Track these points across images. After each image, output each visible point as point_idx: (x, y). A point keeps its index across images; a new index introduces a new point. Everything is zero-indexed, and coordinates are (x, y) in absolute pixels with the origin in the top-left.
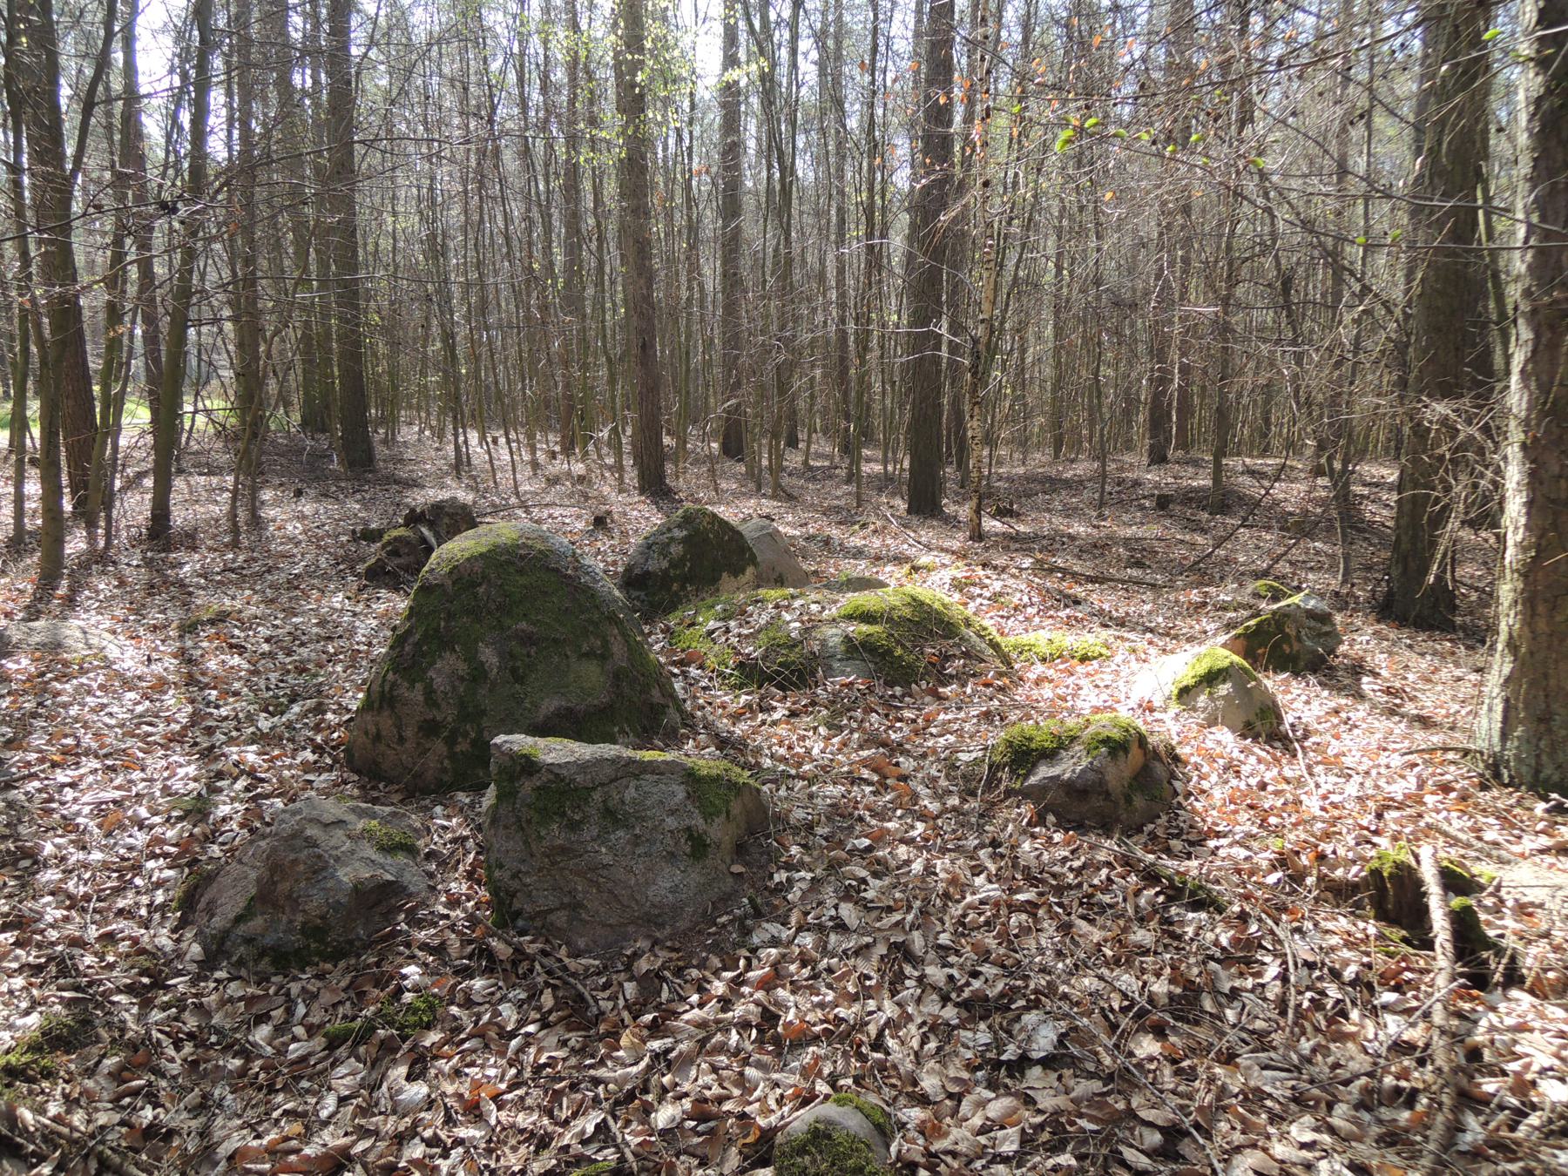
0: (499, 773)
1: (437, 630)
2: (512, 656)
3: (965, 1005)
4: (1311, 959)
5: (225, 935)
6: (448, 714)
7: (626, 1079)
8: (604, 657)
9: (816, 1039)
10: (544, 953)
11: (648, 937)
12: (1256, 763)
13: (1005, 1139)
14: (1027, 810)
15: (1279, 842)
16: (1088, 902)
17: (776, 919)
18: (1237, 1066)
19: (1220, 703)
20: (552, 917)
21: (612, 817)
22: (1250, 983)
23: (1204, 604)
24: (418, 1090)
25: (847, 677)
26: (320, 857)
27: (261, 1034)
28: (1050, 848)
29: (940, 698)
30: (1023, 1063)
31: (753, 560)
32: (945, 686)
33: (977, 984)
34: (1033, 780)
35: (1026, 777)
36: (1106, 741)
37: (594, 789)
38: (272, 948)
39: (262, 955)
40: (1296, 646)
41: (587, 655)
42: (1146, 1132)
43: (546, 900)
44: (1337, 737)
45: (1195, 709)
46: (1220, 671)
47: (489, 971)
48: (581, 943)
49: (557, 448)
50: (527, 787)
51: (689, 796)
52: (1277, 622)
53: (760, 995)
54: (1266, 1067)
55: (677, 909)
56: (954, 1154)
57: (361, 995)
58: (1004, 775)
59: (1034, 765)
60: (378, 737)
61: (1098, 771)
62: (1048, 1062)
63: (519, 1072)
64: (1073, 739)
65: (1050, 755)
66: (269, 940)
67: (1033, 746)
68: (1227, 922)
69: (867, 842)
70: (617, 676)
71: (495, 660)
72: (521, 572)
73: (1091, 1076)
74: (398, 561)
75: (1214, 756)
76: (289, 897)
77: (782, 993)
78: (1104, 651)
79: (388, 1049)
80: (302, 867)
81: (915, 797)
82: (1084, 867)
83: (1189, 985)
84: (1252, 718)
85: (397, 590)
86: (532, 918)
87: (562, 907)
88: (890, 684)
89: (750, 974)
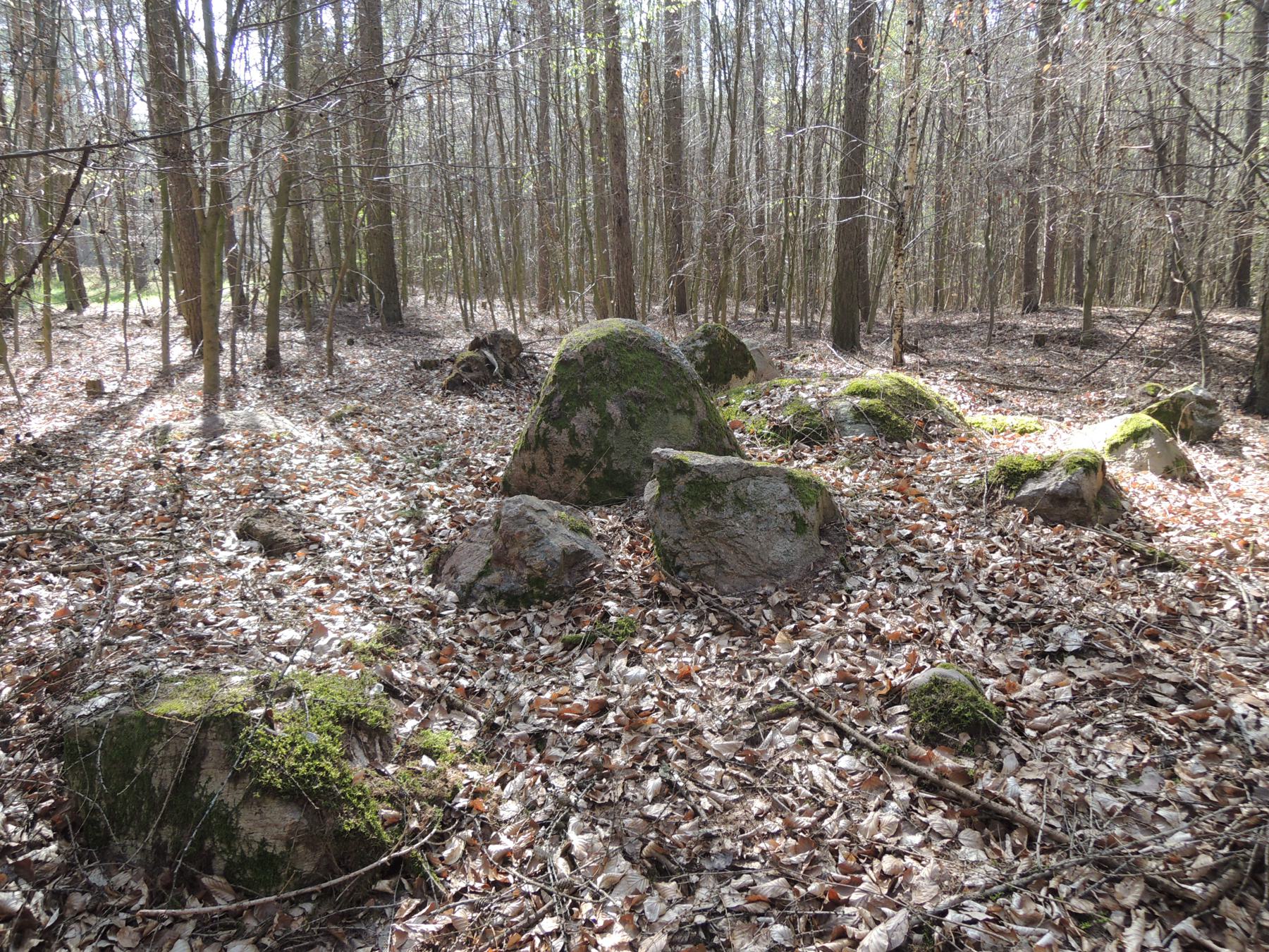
0: (660, 473)
1: (575, 391)
2: (629, 409)
3: (1008, 623)
4: (1259, 595)
5: (472, 585)
6: (587, 450)
7: (786, 660)
8: (691, 413)
9: (908, 641)
10: (703, 592)
11: (772, 584)
12: (1177, 494)
13: (1061, 693)
14: (1021, 514)
15: (1214, 535)
16: (1081, 564)
17: (859, 574)
18: (1219, 654)
19: (1144, 454)
20: (704, 570)
21: (742, 503)
22: (1215, 610)
23: (1103, 402)
24: (637, 671)
25: (859, 435)
26: (538, 530)
27: (516, 642)
28: (1046, 536)
29: (928, 450)
30: (1060, 654)
31: (753, 367)
32: (931, 442)
33: (1014, 611)
34: (1023, 493)
35: (1018, 491)
36: (1081, 463)
37: (728, 483)
38: (506, 594)
39: (498, 599)
40: (1190, 423)
41: (679, 411)
42: (1164, 686)
43: (699, 559)
44: (1236, 480)
45: (1124, 460)
46: (1144, 430)
47: (663, 605)
48: (725, 588)
49: (536, 310)
50: (681, 482)
51: (791, 491)
52: (1174, 405)
53: (862, 615)
54: (1239, 655)
55: (790, 567)
56: (1028, 700)
57: (578, 620)
58: (1000, 491)
59: (1024, 482)
60: (533, 470)
61: (1076, 484)
62: (1077, 654)
63: (707, 659)
64: (1053, 463)
65: (1035, 475)
66: (504, 588)
67: (1022, 469)
68: (1191, 576)
69: (908, 532)
70: (701, 427)
71: (618, 412)
72: (630, 351)
73: (1112, 660)
74: (470, 375)
75: (1143, 488)
76: (518, 558)
77: (877, 616)
78: (1038, 426)
79: (609, 649)
80: (526, 537)
81: (934, 508)
82: (1074, 546)
83: (1171, 611)
84: (1171, 465)
85: (472, 396)
86: (689, 571)
87: (711, 563)
88: (890, 440)
89: (850, 605)
